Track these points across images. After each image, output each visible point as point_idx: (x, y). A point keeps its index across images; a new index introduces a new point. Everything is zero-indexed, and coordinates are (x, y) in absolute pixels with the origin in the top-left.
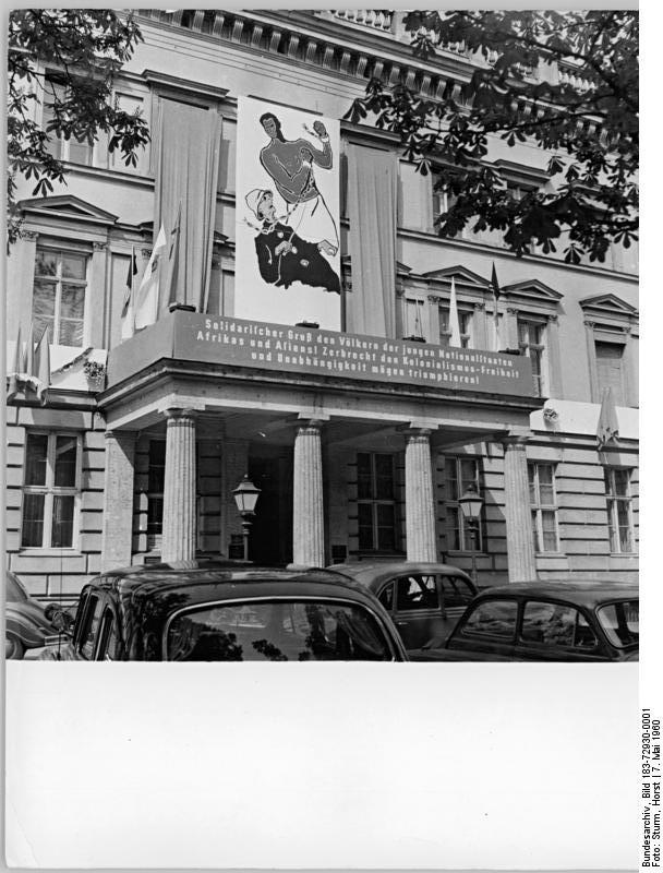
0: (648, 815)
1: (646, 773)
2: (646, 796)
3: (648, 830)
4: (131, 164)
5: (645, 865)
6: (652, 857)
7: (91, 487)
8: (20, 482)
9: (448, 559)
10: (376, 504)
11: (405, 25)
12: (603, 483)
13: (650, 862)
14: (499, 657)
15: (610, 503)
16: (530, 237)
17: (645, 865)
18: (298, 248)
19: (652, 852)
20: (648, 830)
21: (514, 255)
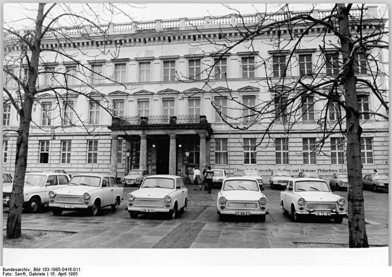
0: (26, 270)
1: (45, 269)
2: (35, 269)
3: (19, 270)
5: (4, 269)
6: (7, 272)
7: (383, 170)
8: (228, 153)
9: (30, 223)
10: (286, 158)
11: (43, 201)
12: (110, 144)
13: (5, 271)
17: (4, 269)
19: (9, 272)
20: (19, 270)
21: (49, 183)
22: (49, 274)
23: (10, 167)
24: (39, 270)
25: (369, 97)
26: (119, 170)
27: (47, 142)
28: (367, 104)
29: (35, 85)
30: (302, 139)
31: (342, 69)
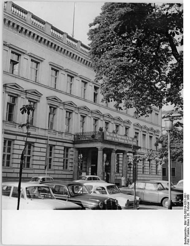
0: (186, 230)
1: (185, 218)
2: (185, 224)
3: (186, 234)
4: (102, 102)
5: (185, 244)
6: (187, 242)
12: (63, 151)
13: (187, 243)
14: (109, 157)
15: (64, 160)
16: (81, 153)
17: (185, 244)
18: (106, 178)
19: (187, 240)
20: (186, 234)
22: (188, 217)
23: (130, 171)
24: (185, 221)
25: (15, 106)
26: (148, 170)
27: (67, 148)
28: (4, 145)
29: (91, 169)
30: (63, 147)
31: (176, 67)
